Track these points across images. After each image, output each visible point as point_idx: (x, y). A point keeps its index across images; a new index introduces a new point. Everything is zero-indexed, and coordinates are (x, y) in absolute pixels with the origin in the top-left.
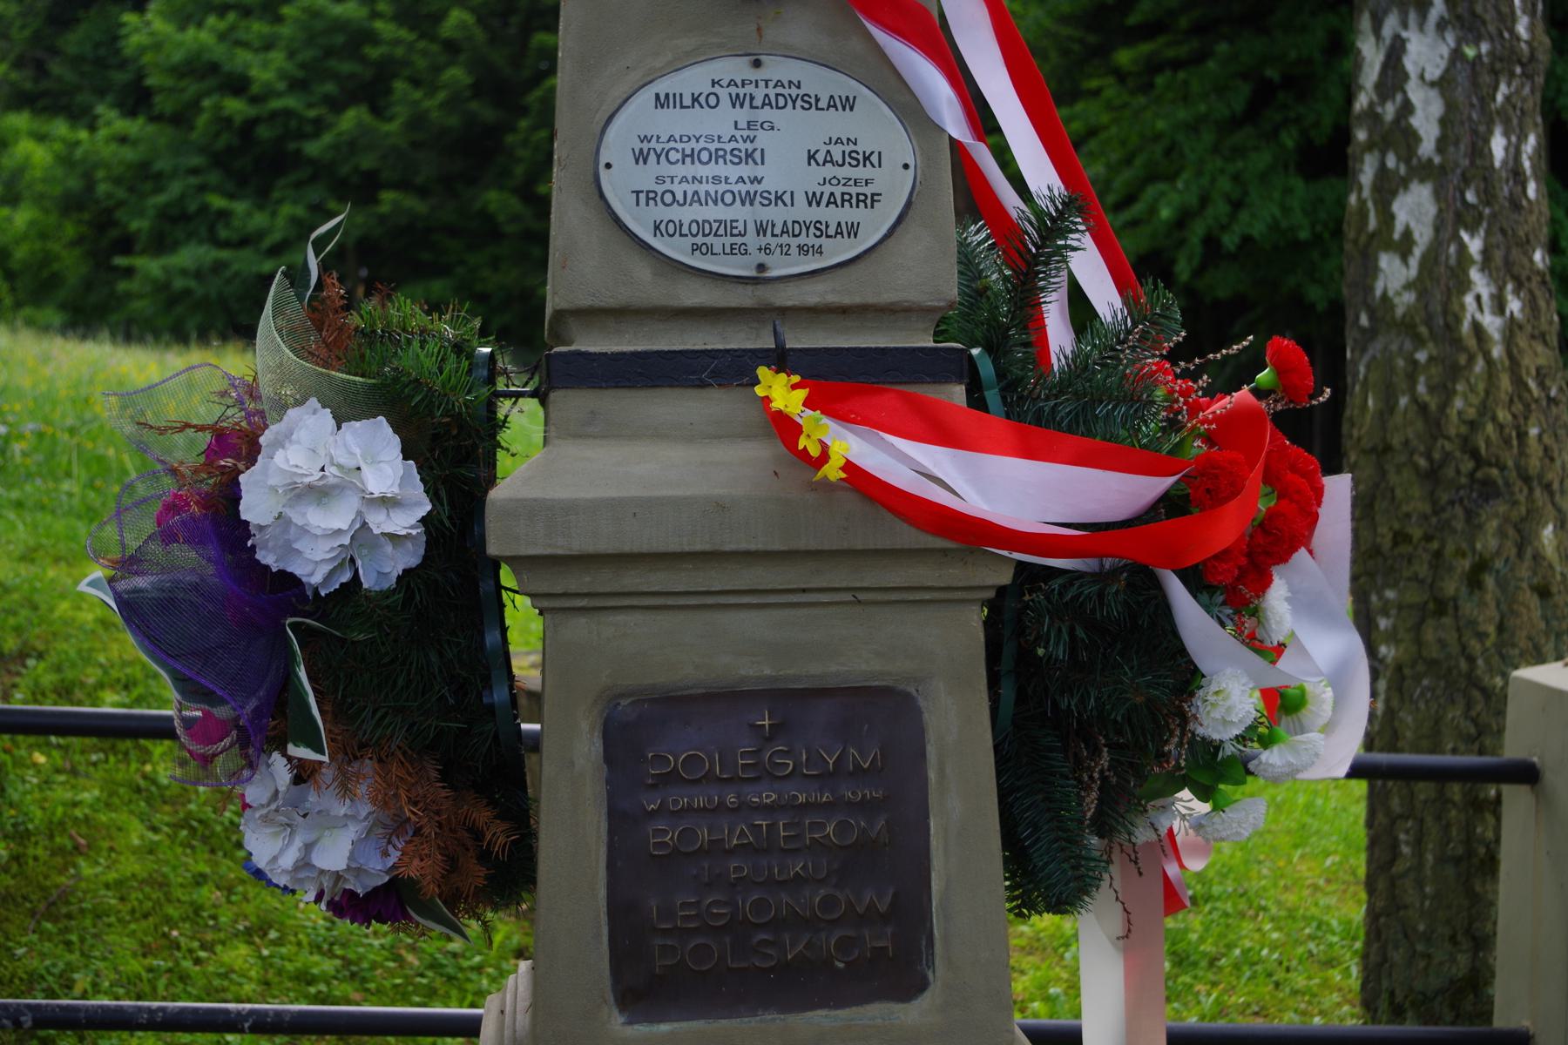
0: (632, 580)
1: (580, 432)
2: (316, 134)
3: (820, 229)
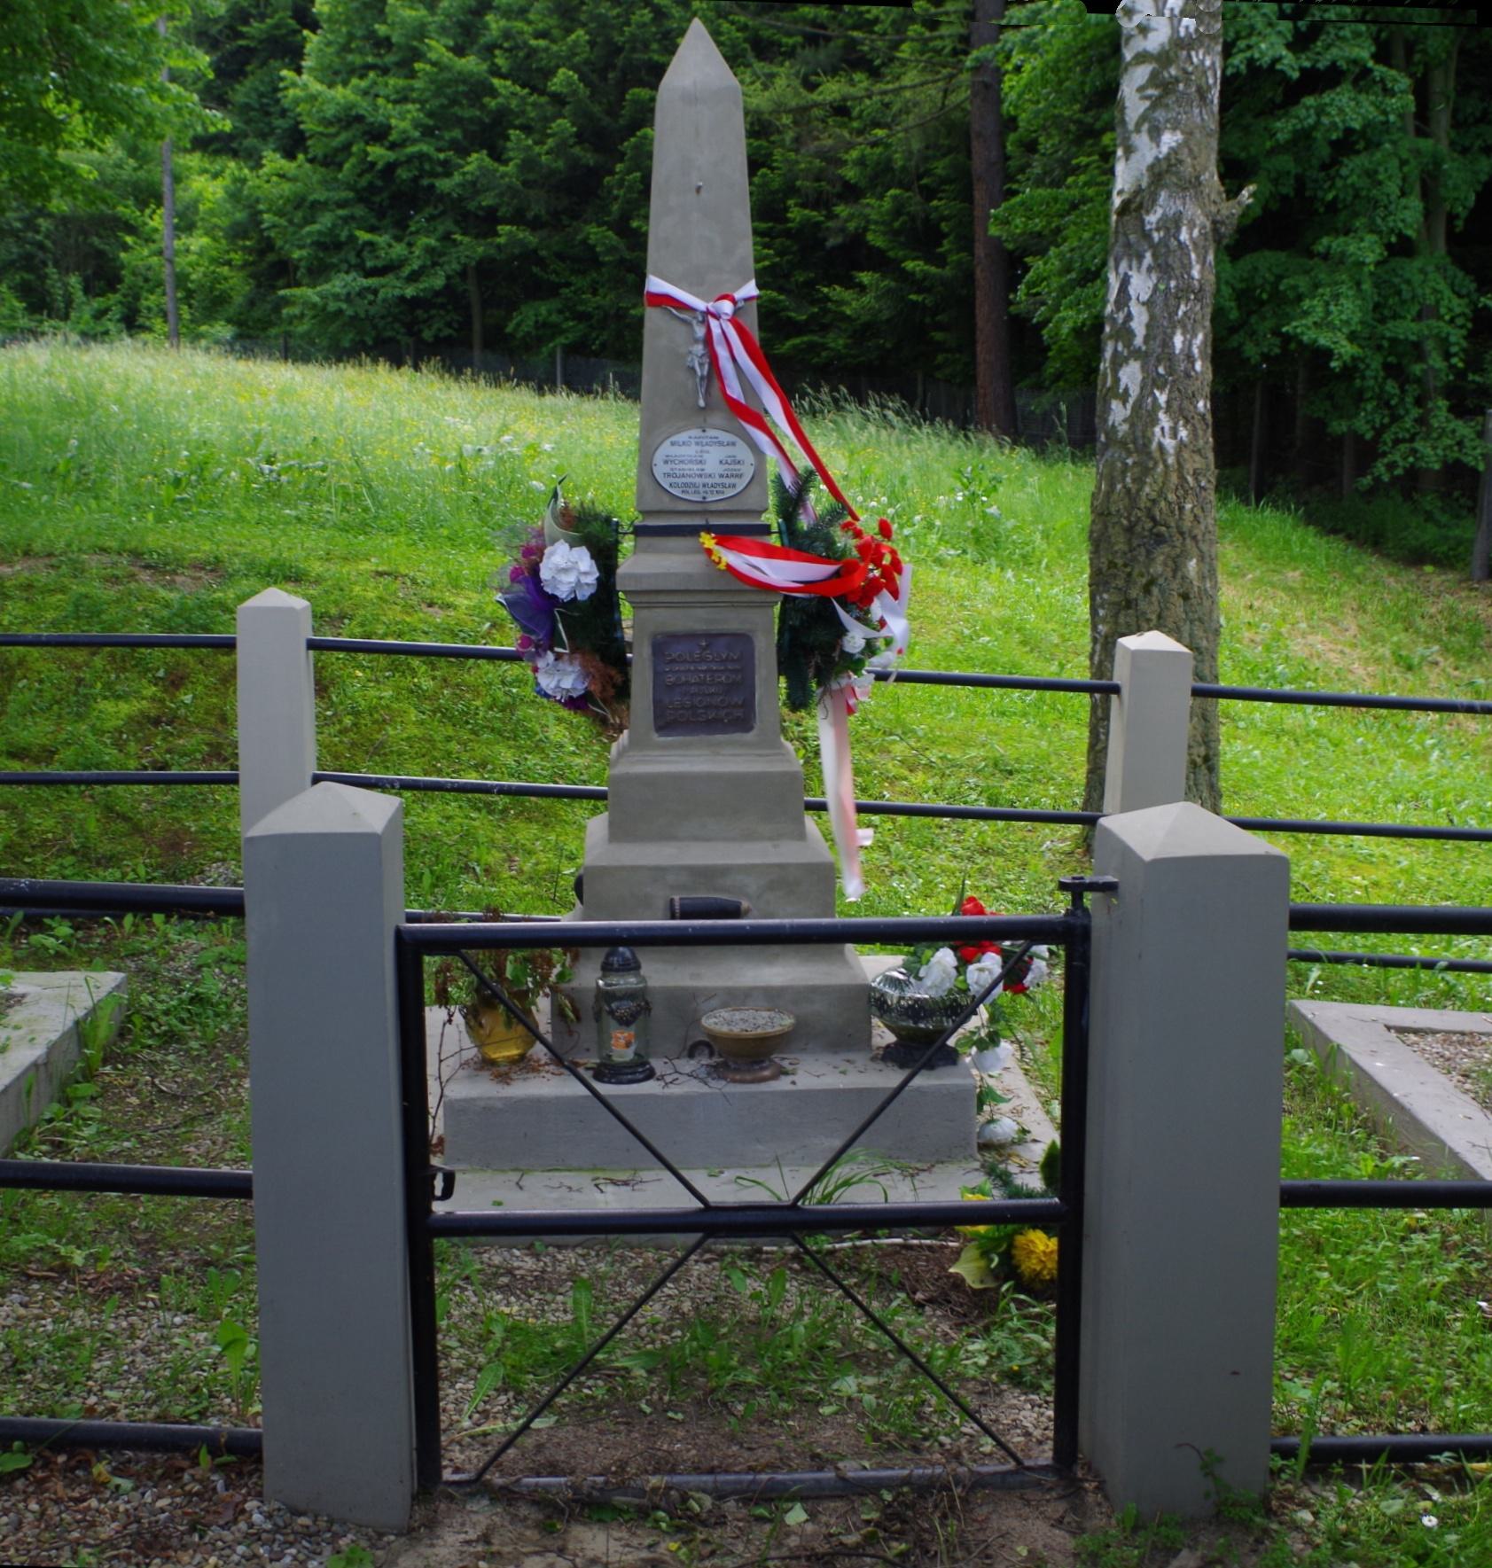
0: (662, 598)
1: (645, 551)
2: (448, 174)
3: (724, 485)
